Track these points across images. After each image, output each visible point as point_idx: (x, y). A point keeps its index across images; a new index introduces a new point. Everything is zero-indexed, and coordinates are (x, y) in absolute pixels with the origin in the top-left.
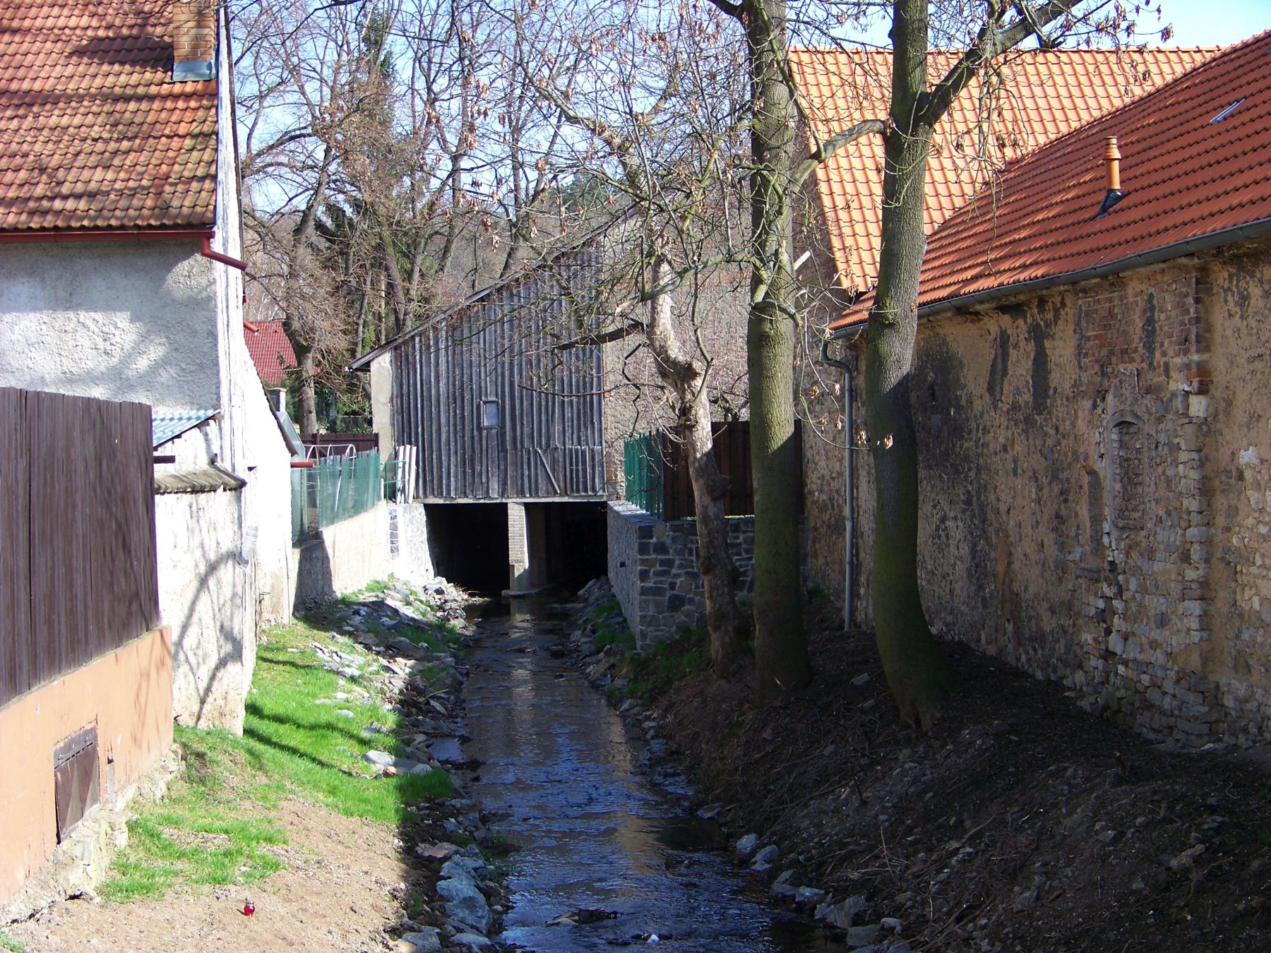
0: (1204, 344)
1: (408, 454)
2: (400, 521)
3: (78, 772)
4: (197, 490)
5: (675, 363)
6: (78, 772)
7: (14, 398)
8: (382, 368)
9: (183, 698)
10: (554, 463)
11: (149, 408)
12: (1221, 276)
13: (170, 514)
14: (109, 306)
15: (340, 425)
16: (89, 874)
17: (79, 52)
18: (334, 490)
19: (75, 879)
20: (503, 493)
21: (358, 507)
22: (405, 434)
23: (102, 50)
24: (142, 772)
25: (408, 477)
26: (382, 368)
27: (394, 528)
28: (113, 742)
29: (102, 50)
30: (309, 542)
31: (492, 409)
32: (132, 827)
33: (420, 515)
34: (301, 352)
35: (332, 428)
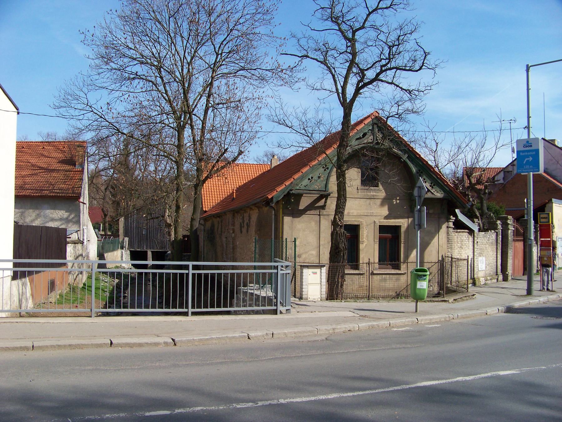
0: (234, 226)
1: (127, 239)
2: (124, 253)
3: (52, 285)
4: (75, 243)
5: (168, 223)
6: (52, 285)
7: (17, 210)
8: (122, 220)
9: (71, 278)
10: (158, 242)
11: (65, 230)
12: (236, 214)
13: (70, 248)
14: (61, 210)
15: (114, 232)
16: (53, 300)
17: (59, 162)
18: (107, 246)
19: (50, 300)
20: (147, 249)
21: (113, 250)
22: (126, 235)
23: (63, 162)
24: (62, 289)
25: (126, 244)
26: (122, 220)
27: (122, 255)
28: (57, 283)
29: (63, 162)
30: (101, 256)
31: (145, 230)
32: (60, 295)
33: (129, 252)
34: (105, 215)
35: (112, 233)
